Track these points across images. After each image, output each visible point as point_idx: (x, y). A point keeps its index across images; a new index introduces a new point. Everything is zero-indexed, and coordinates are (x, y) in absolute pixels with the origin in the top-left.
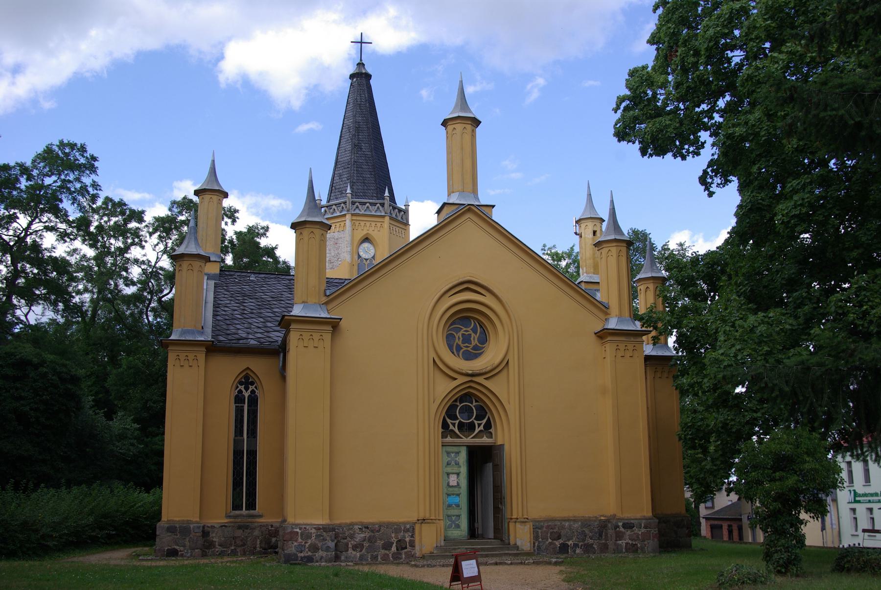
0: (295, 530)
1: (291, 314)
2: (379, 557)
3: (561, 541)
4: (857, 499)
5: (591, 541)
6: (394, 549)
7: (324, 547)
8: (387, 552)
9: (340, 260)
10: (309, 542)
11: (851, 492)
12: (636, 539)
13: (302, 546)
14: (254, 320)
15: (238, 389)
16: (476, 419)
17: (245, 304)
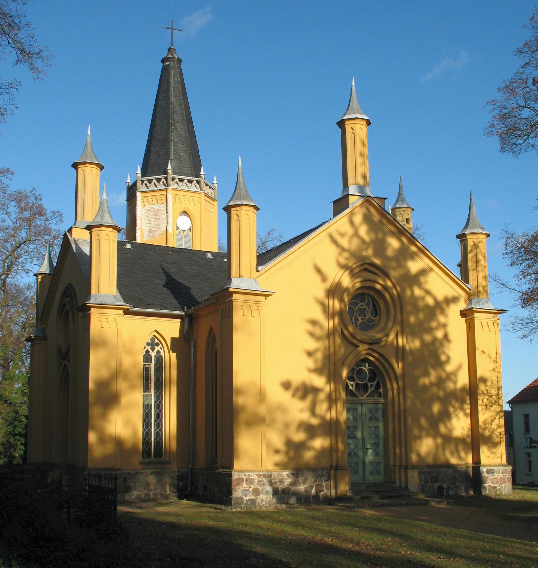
0: (241, 477)
2: (303, 499)
3: (438, 484)
4: (533, 445)
7: (265, 491)
10: (253, 487)
11: (527, 440)
13: (247, 490)
15: (146, 349)
16: (369, 381)
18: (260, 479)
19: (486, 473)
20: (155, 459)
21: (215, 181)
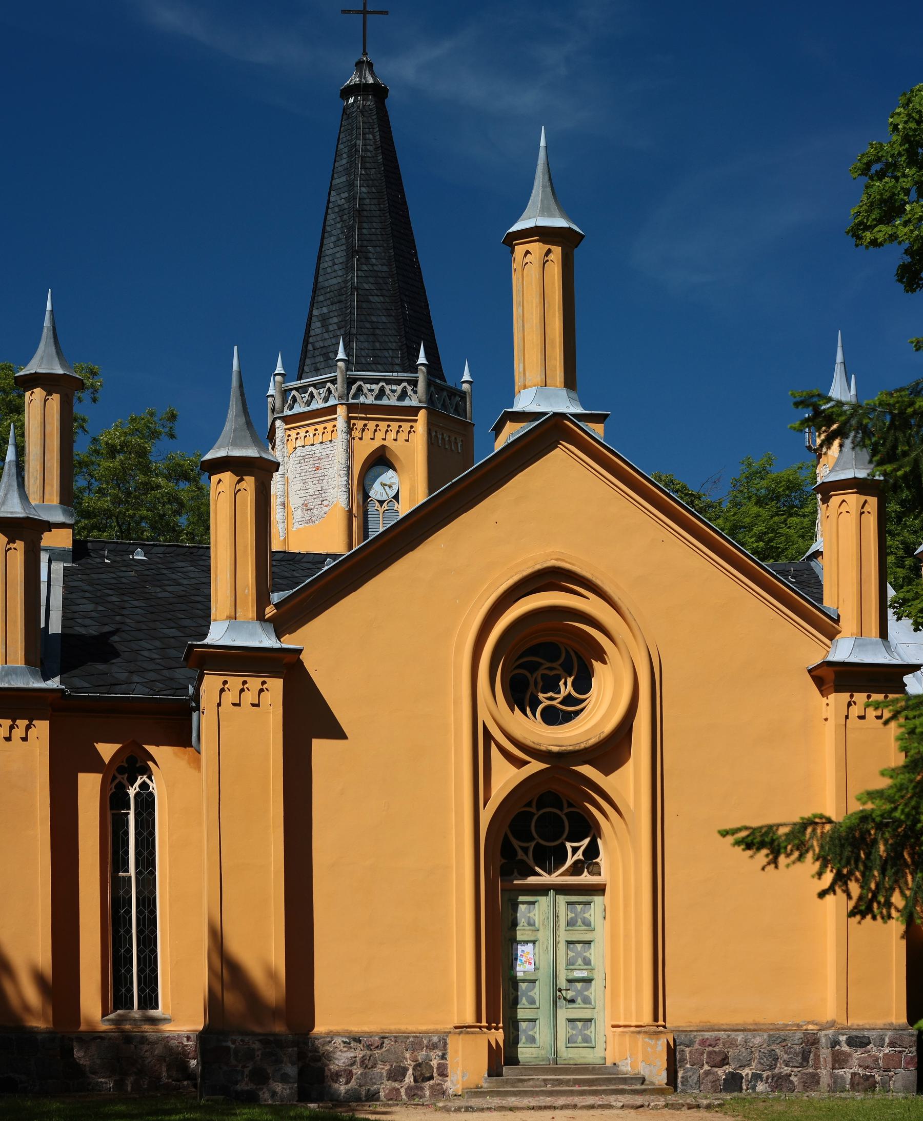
1: (205, 642)
3: (728, 1069)
5: (786, 1070)
6: (409, 1079)
8: (396, 1085)
9: (325, 503)
12: (873, 1065)
14: (143, 644)
15: (117, 781)
17: (125, 612)
18: (267, 1050)
19: (845, 1045)
20: (140, 1012)
21: (466, 377)
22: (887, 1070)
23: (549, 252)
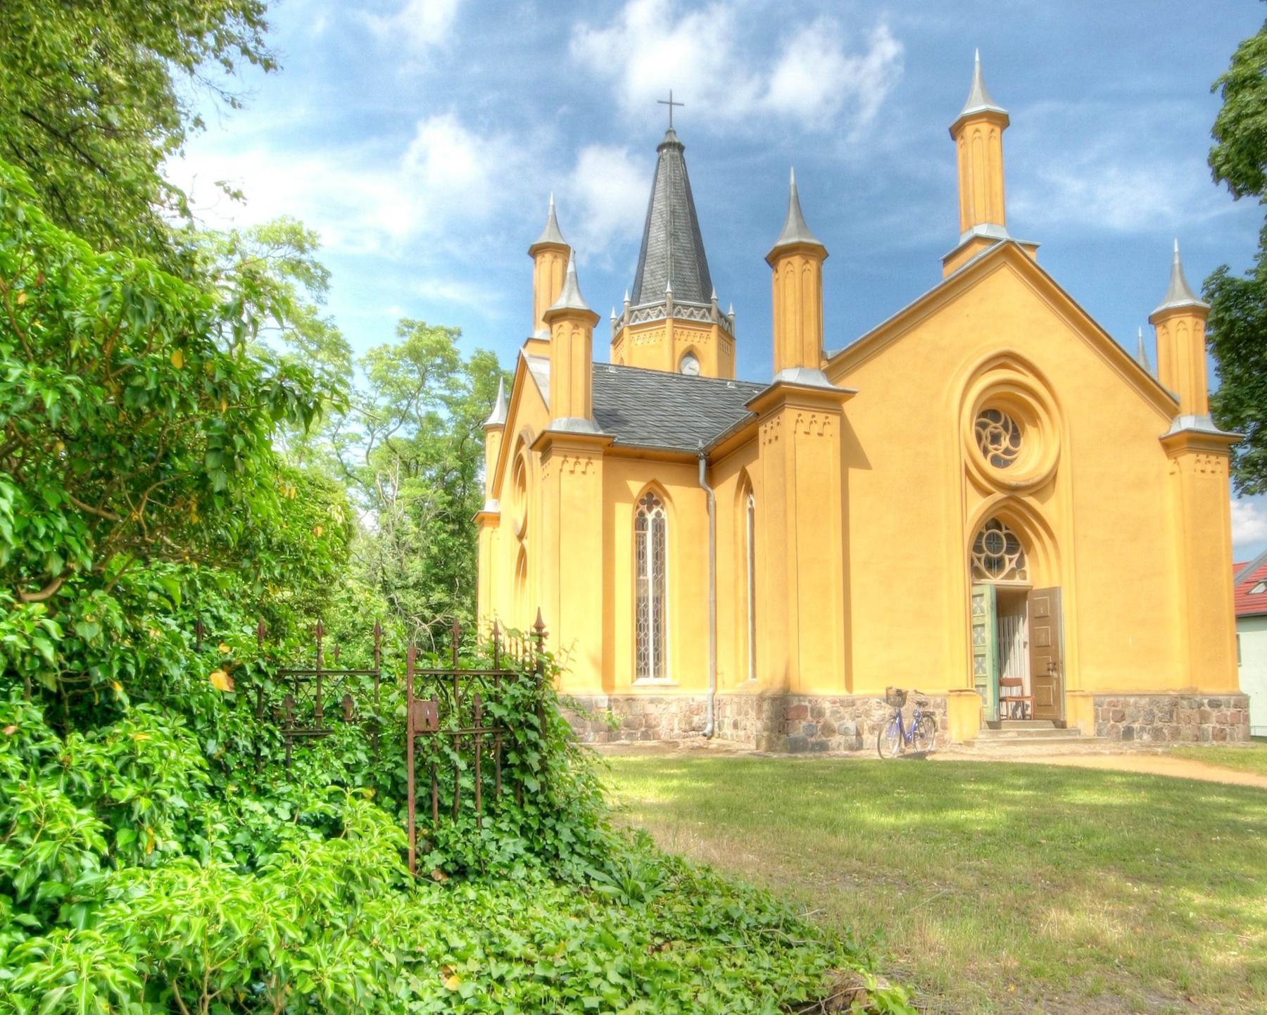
3: (1125, 723)
5: (1160, 724)
22: (1232, 725)
23: (992, 131)
